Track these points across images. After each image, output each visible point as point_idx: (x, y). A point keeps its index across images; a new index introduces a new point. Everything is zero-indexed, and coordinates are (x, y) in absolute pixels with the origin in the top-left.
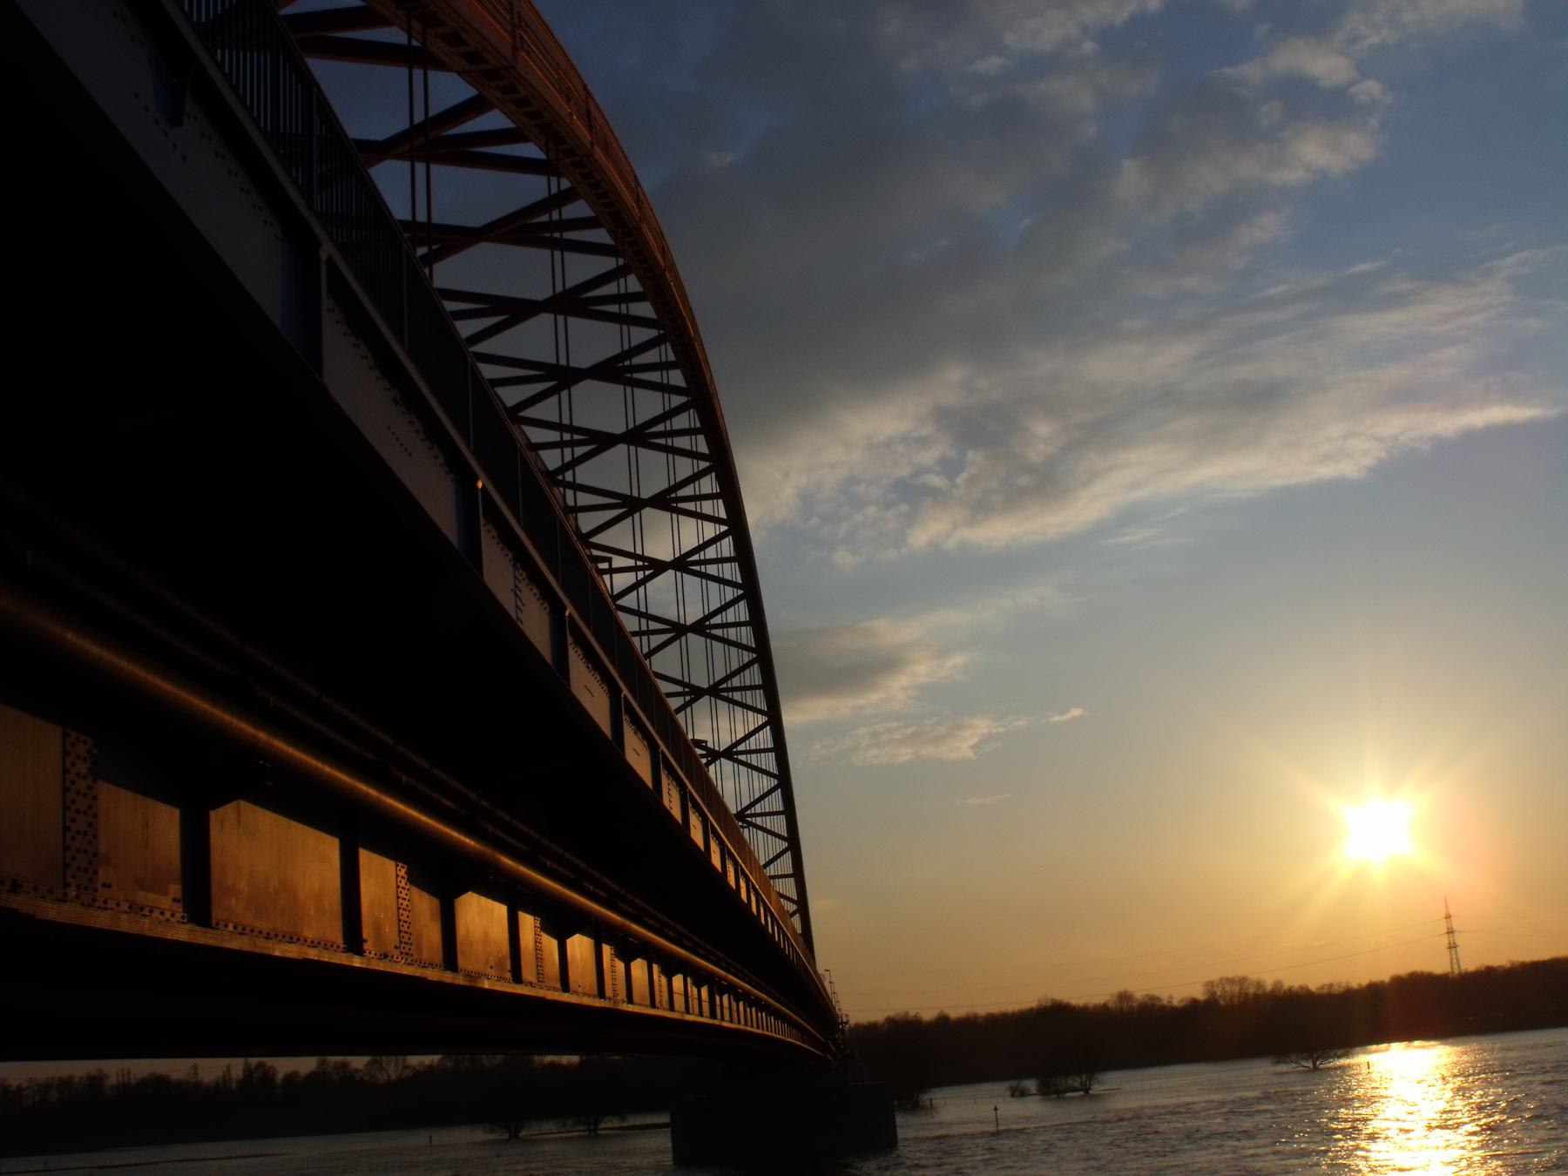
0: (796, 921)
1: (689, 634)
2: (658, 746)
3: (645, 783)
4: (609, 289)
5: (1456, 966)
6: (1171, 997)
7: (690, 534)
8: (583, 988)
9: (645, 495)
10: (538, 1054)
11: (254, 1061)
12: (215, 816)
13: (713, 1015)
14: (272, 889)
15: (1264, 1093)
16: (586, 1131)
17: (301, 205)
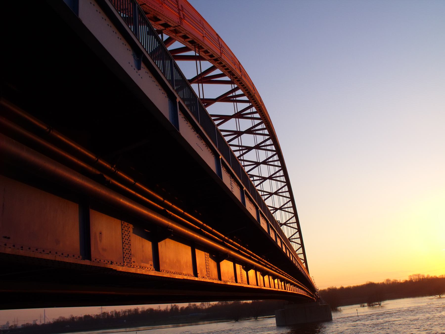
0: (304, 264)
4: (248, 111)
6: (400, 280)
7: (272, 170)
10: (242, 301)
11: (173, 304)
12: (159, 244)
13: (285, 289)
14: (175, 262)
15: (427, 304)
16: (254, 319)
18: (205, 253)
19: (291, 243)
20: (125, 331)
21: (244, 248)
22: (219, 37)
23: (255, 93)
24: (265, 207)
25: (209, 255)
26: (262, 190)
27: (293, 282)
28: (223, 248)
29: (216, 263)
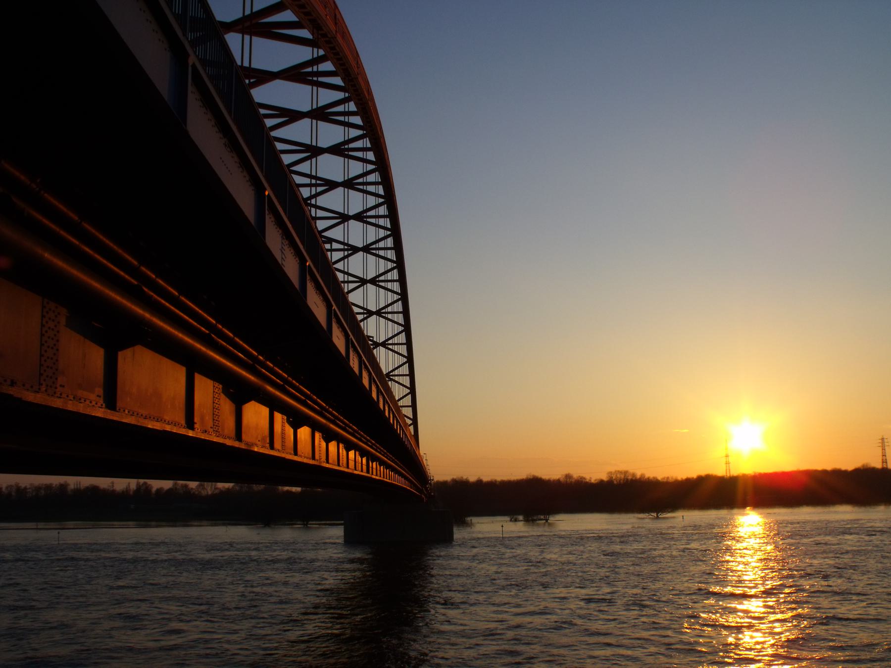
0: (412, 428)
1: (368, 284)
2: (362, 357)
3: (319, 322)
4: (340, 108)
5: (728, 473)
6: (591, 478)
7: (372, 234)
8: (305, 455)
9: (351, 214)
11: (142, 481)
12: (121, 355)
13: (368, 472)
16: (302, 525)
17: (179, 33)
18: (215, 383)
19: (390, 383)
20: (36, 527)
21: (294, 382)
22: (337, 8)
23: (358, 74)
24: (346, 307)
25: (221, 388)
26: (346, 270)
27: (386, 459)
28: (252, 378)
29: (234, 405)
